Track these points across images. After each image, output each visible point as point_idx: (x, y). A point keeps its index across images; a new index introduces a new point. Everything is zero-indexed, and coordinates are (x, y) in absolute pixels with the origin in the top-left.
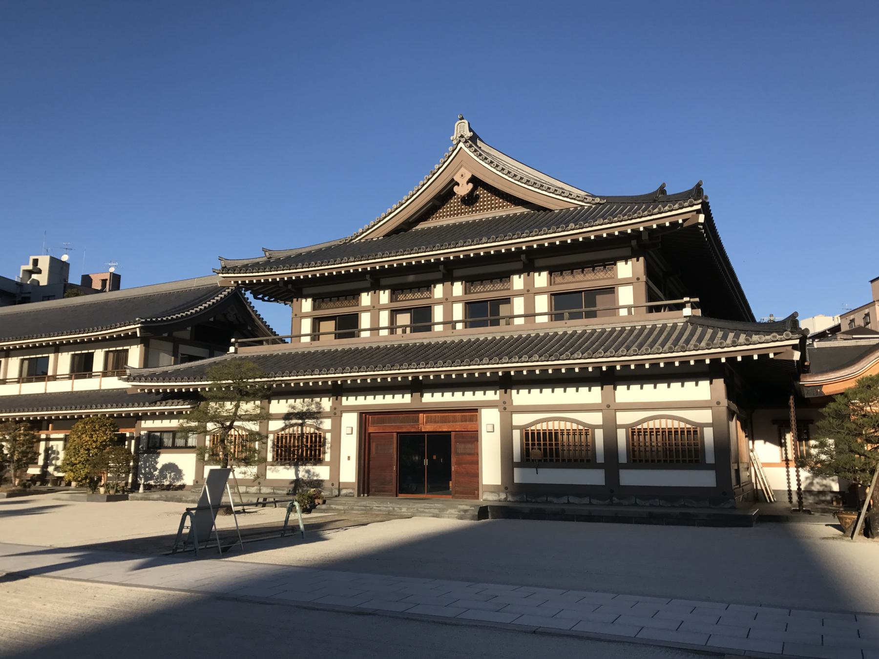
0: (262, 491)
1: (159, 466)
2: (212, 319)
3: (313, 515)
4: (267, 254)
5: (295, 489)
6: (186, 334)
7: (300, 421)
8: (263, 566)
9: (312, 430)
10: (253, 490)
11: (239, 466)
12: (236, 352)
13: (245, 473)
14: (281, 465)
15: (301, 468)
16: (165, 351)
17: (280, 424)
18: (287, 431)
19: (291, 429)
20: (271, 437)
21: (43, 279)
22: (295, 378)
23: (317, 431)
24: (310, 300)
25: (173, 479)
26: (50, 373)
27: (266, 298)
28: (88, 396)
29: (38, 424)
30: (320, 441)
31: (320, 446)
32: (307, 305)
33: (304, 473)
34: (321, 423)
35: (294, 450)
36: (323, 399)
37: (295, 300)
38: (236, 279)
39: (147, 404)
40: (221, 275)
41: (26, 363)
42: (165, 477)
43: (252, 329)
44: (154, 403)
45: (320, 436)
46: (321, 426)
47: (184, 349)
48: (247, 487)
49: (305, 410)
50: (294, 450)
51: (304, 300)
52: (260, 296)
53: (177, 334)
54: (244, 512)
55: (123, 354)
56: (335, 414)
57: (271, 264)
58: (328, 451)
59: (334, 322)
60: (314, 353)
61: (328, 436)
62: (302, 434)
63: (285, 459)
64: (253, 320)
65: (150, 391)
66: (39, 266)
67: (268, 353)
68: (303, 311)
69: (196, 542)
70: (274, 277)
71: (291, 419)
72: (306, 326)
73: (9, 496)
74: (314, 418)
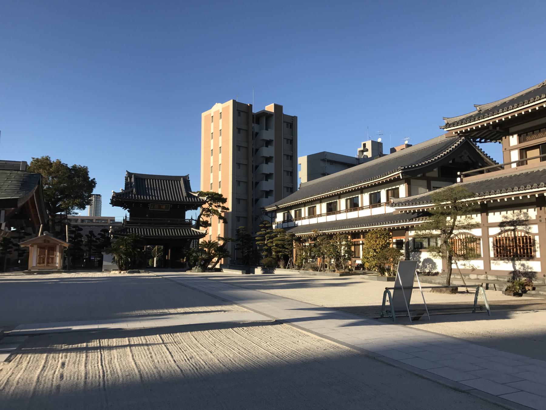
0: (489, 279)
1: (422, 260)
2: (451, 162)
3: (524, 298)
4: (478, 108)
5: (514, 278)
6: (435, 173)
7: (512, 228)
8: (434, 335)
9: (523, 234)
10: (482, 277)
11: (459, 260)
12: (462, 181)
13: (465, 265)
14: (501, 260)
15: (517, 263)
16: (423, 187)
17: (497, 230)
18: (503, 235)
19: (506, 234)
20: (491, 240)
21: (369, 154)
22: (500, 195)
23: (526, 235)
24: (516, 136)
25: (431, 268)
26: (360, 206)
27: (483, 141)
28: (378, 218)
29: (355, 235)
30: (530, 242)
31: (531, 246)
32: (514, 140)
33: (520, 266)
34: (530, 228)
35: (510, 249)
36: (529, 210)
37: (504, 138)
38: (456, 131)
39: (408, 220)
40: (445, 130)
41: (349, 201)
42: (426, 267)
43: (479, 163)
44: (411, 220)
45: (530, 239)
46: (530, 231)
47: (433, 183)
48: (477, 275)
49: (515, 219)
50: (510, 249)
51: (511, 137)
52: (478, 140)
53: (428, 174)
54: (467, 292)
55: (396, 191)
56: (541, 221)
57: (480, 115)
58: (538, 250)
59: (538, 150)
60: (519, 175)
61: (537, 238)
62: (515, 237)
63: (504, 256)
64: (482, 159)
65: (410, 211)
66: (367, 147)
67: (484, 180)
68: (511, 145)
69: (393, 311)
70: (482, 124)
71: (505, 226)
72: (515, 156)
73: (341, 275)
74: (523, 225)
